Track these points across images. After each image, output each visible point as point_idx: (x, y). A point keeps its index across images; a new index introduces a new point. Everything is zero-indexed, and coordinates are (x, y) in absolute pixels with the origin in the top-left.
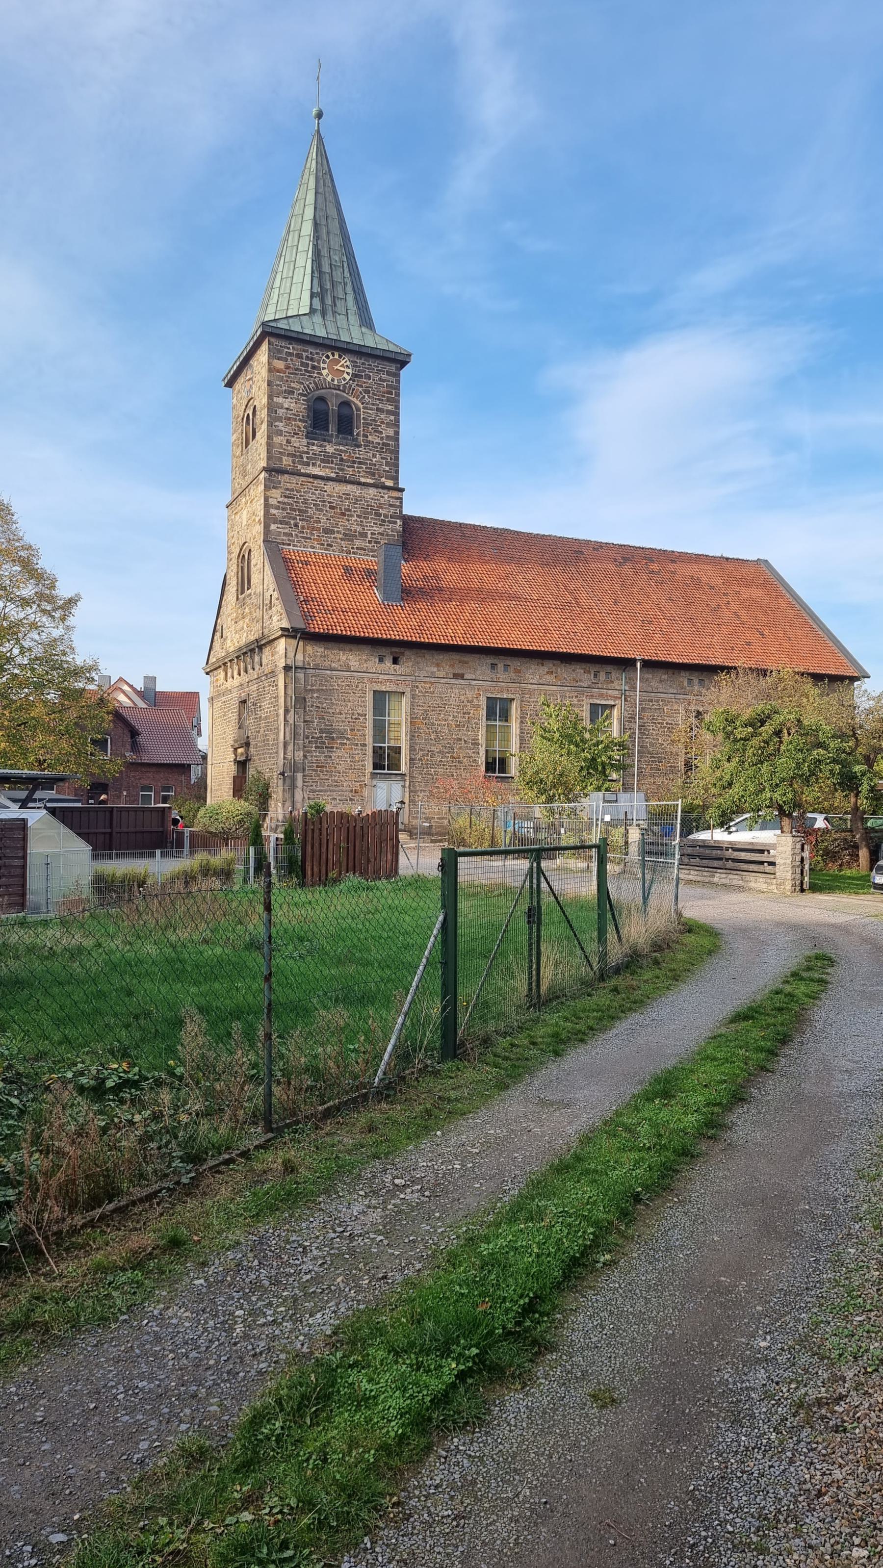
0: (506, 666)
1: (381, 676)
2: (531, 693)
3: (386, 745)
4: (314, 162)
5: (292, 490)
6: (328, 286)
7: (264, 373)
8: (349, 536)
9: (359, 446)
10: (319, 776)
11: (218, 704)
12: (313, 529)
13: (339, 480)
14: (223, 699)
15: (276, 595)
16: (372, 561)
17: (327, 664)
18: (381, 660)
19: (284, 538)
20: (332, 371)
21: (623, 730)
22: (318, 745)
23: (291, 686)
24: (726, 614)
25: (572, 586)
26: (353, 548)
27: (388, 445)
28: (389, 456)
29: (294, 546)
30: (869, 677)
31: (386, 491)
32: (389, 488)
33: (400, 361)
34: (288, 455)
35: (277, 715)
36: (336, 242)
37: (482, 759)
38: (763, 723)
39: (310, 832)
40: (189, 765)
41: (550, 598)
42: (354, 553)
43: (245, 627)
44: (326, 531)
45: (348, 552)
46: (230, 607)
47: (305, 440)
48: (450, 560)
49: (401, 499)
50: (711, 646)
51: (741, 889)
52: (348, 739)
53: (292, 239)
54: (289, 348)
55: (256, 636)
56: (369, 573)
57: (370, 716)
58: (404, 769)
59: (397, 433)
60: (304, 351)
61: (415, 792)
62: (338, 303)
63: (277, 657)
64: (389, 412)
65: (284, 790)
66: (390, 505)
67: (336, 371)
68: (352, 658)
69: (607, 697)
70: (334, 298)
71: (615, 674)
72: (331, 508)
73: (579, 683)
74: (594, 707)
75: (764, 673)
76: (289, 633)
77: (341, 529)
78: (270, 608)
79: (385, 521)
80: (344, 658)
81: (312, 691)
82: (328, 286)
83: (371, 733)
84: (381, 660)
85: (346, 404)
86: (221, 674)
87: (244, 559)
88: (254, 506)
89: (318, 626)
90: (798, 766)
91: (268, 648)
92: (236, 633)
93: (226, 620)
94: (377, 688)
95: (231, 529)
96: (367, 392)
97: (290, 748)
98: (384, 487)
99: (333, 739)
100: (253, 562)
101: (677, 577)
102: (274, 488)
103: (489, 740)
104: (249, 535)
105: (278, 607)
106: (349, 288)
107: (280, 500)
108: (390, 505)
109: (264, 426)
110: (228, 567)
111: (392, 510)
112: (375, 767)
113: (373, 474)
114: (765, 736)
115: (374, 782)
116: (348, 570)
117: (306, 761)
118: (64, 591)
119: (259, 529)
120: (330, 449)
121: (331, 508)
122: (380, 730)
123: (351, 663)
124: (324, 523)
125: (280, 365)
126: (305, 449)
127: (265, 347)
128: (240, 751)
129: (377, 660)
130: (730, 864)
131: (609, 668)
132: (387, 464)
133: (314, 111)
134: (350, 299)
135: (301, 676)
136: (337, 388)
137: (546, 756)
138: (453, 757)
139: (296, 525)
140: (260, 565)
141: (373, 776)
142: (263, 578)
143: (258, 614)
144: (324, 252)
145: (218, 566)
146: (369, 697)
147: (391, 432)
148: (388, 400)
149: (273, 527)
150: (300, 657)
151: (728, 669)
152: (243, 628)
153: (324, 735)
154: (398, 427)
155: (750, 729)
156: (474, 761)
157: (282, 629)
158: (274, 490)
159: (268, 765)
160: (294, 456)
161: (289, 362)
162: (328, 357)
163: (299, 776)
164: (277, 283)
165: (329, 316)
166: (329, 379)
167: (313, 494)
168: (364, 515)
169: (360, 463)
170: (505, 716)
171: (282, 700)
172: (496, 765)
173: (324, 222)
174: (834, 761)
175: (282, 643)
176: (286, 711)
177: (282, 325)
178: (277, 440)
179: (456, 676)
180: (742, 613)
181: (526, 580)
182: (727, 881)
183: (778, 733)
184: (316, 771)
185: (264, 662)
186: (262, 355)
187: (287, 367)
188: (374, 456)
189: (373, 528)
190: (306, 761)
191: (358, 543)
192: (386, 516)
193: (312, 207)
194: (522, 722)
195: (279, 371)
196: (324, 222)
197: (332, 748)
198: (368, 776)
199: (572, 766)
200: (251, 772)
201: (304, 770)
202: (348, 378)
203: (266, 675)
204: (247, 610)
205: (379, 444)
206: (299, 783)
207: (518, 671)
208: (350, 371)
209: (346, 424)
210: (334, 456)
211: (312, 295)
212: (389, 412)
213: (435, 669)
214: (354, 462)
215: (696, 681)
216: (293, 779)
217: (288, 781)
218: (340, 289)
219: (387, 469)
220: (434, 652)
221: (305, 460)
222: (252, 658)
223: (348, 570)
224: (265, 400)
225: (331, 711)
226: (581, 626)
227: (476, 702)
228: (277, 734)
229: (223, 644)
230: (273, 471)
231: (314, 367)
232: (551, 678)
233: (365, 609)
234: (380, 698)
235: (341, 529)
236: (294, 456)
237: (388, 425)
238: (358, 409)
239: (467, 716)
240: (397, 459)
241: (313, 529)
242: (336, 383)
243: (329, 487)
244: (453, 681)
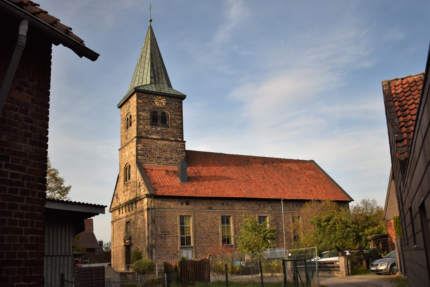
0: (227, 204)
1: (182, 210)
2: (237, 213)
4: (150, 36)
5: (146, 144)
6: (156, 74)
7: (135, 104)
8: (167, 159)
9: (169, 127)
11: (115, 224)
12: (154, 157)
13: (163, 139)
14: (118, 221)
15: (142, 182)
16: (176, 168)
17: (162, 206)
18: (182, 204)
20: (159, 102)
21: (271, 225)
23: (150, 216)
24: (303, 180)
25: (247, 173)
30: (353, 201)
32: (180, 141)
34: (144, 132)
35: (145, 227)
36: (158, 60)
37: (221, 239)
38: (329, 221)
39: (183, 268)
40: (95, 249)
41: (240, 178)
43: (128, 194)
44: (158, 158)
45: (166, 165)
46: (121, 186)
48: (203, 166)
50: (299, 193)
51: (329, 277)
52: (171, 234)
53: (143, 60)
55: (134, 197)
56: (175, 172)
57: (179, 225)
58: (192, 244)
61: (197, 253)
62: (160, 80)
63: (144, 205)
64: (179, 115)
65: (148, 256)
67: (160, 103)
68: (171, 204)
69: (264, 213)
70: (159, 78)
71: (266, 205)
72: (160, 149)
74: (260, 217)
75: (320, 201)
76: (147, 196)
77: (164, 157)
78: (140, 187)
80: (169, 204)
81: (158, 217)
82: (156, 74)
83: (180, 231)
84: (182, 204)
85: (164, 113)
86: (117, 212)
87: (127, 169)
88: (132, 149)
89: (159, 192)
90: (343, 234)
91: (139, 201)
92: (124, 196)
93: (120, 192)
94: (181, 215)
95: (121, 158)
96: (171, 109)
97: (150, 239)
98: (179, 141)
99: (166, 235)
100: (131, 170)
101: (283, 168)
103: (223, 232)
104: (129, 160)
105: (143, 187)
106: (163, 75)
109: (135, 122)
110: (120, 172)
111: (182, 149)
112: (182, 244)
113: (174, 137)
114: (331, 225)
115: (181, 251)
116: (167, 171)
118: (66, 184)
119: (135, 158)
120: (159, 129)
121: (160, 149)
122: (183, 230)
123: (171, 206)
124: (158, 155)
125: (140, 101)
127: (135, 95)
128: (127, 241)
130: (324, 269)
131: (264, 202)
133: (149, 20)
134: (164, 79)
135: (153, 211)
136: (161, 108)
137: (249, 237)
138: (210, 239)
139: (148, 156)
140: (135, 171)
141: (181, 248)
142: (136, 175)
143: (134, 189)
144: (154, 64)
145: (115, 171)
146: (178, 218)
147: (180, 122)
148: (179, 111)
149: (139, 157)
150: (153, 204)
151: (308, 201)
152: (127, 194)
154: (182, 120)
155: (326, 223)
156: (218, 240)
157: (146, 195)
159: (141, 246)
160: (146, 132)
162: (157, 98)
163: (154, 250)
164: (138, 74)
165: (157, 84)
166: (158, 105)
168: (172, 151)
170: (228, 222)
171: (146, 221)
172: (226, 240)
173: (154, 54)
174: (353, 231)
175: (146, 200)
176: (148, 225)
177: (141, 88)
178: (140, 127)
180: (308, 180)
181: (230, 171)
182: (323, 275)
183: (335, 224)
185: (138, 206)
186: (134, 99)
187: (143, 102)
188: (174, 130)
189: (175, 156)
191: (170, 161)
192: (179, 151)
193: (150, 49)
194: (234, 224)
195: (140, 103)
196: (154, 54)
199: (258, 240)
200: (133, 249)
201: (155, 247)
202: (164, 104)
203: (139, 212)
204: (129, 188)
206: (154, 252)
207: (232, 205)
209: (164, 120)
210: (160, 131)
211: (151, 78)
212: (179, 115)
213: (202, 206)
214: (167, 133)
215: (295, 206)
216: (152, 251)
217: (150, 252)
218: (160, 75)
222: (132, 206)
223: (167, 171)
224: (135, 113)
225: (164, 224)
226: (253, 188)
227: (217, 218)
228: (145, 234)
229: (117, 201)
230: (139, 138)
231: (152, 101)
232: (243, 207)
233: (173, 185)
234: (182, 218)
235: (164, 157)
236: (146, 132)
237: (179, 120)
238: (168, 115)
240: (183, 131)
241: (154, 157)
243: (159, 142)
244: (208, 210)
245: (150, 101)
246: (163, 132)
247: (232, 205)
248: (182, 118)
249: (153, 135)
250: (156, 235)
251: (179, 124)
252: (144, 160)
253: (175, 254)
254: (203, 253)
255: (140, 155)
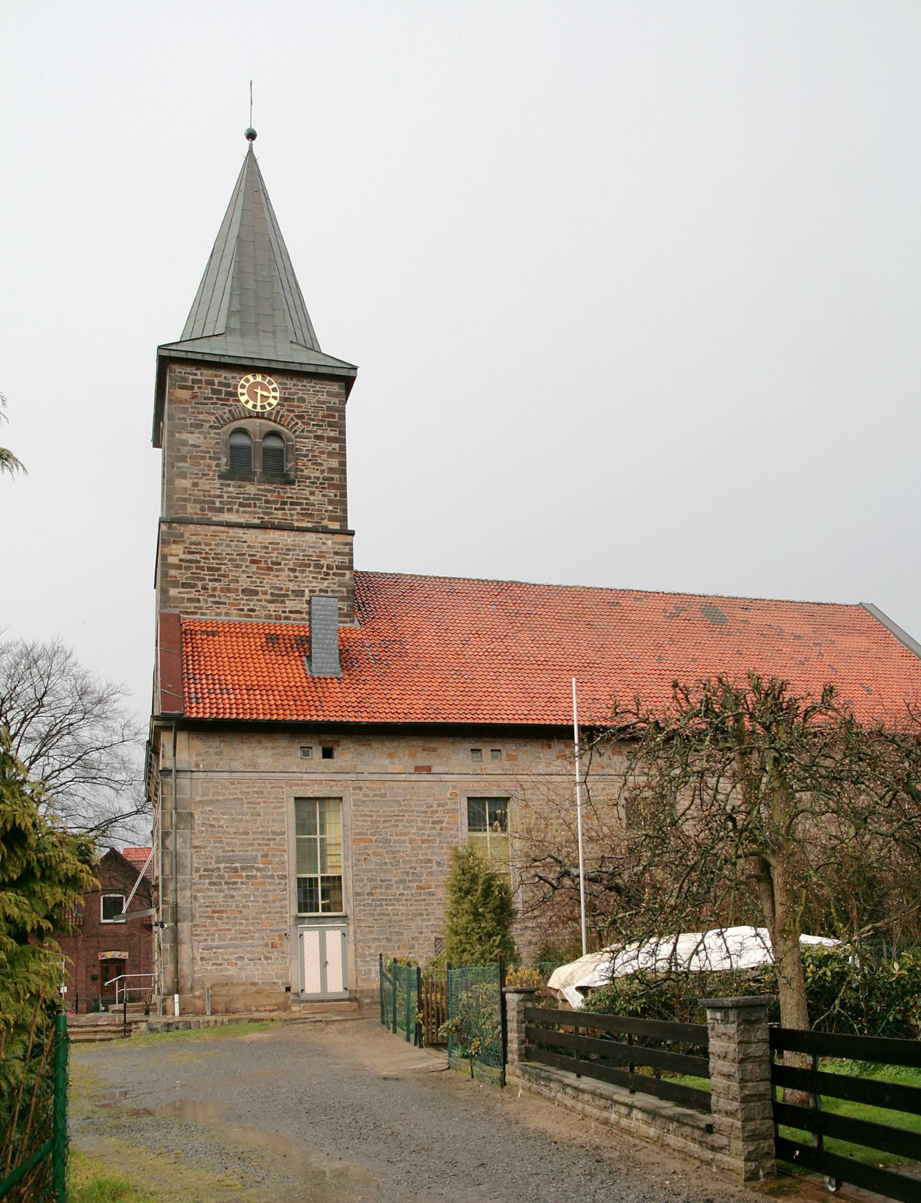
3: (319, 875)
5: (199, 544)
10: (216, 925)
13: (263, 527)
18: (306, 752)
19: (188, 605)
22: (214, 880)
26: (284, 612)
27: (332, 479)
28: (331, 493)
29: (202, 614)
31: (329, 536)
32: (334, 532)
33: (344, 379)
34: (196, 501)
42: (287, 618)
47: (217, 481)
49: (351, 544)
52: (259, 869)
54: (196, 375)
59: (343, 464)
60: (216, 376)
64: (330, 440)
66: (336, 553)
67: (259, 395)
73: (606, 771)
77: (267, 588)
79: (328, 574)
84: (306, 752)
99: (235, 870)
102: (175, 542)
107: (182, 556)
108: (336, 553)
111: (338, 558)
112: (302, 907)
117: (196, 904)
120: (251, 489)
121: (254, 562)
122: (307, 852)
124: (245, 583)
126: (218, 492)
129: (299, 753)
132: (331, 502)
136: (259, 416)
147: (334, 463)
149: (173, 592)
153: (222, 865)
158: (174, 546)
161: (196, 390)
162: (247, 381)
166: (249, 406)
167: (228, 546)
169: (292, 504)
179: (419, 770)
184: (212, 918)
190: (196, 904)
195: (181, 401)
197: (235, 883)
198: (291, 921)
201: (193, 917)
202: (274, 402)
205: (318, 478)
208: (277, 394)
211: (230, 313)
213: (387, 762)
214: (285, 503)
219: (331, 508)
220: (384, 738)
221: (218, 505)
231: (227, 393)
235: (267, 588)
237: (331, 455)
239: (438, 826)
242: (259, 409)
244: (415, 777)
245: (220, 392)
246: (267, 502)
247: (515, 758)
248: (343, 449)
249: (230, 510)
250: (197, 870)
251: (331, 470)
252: (191, 600)
253: (273, 946)
254: (389, 940)
255: (175, 584)
